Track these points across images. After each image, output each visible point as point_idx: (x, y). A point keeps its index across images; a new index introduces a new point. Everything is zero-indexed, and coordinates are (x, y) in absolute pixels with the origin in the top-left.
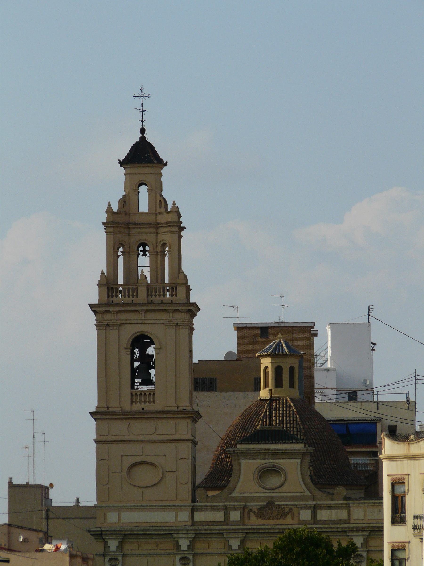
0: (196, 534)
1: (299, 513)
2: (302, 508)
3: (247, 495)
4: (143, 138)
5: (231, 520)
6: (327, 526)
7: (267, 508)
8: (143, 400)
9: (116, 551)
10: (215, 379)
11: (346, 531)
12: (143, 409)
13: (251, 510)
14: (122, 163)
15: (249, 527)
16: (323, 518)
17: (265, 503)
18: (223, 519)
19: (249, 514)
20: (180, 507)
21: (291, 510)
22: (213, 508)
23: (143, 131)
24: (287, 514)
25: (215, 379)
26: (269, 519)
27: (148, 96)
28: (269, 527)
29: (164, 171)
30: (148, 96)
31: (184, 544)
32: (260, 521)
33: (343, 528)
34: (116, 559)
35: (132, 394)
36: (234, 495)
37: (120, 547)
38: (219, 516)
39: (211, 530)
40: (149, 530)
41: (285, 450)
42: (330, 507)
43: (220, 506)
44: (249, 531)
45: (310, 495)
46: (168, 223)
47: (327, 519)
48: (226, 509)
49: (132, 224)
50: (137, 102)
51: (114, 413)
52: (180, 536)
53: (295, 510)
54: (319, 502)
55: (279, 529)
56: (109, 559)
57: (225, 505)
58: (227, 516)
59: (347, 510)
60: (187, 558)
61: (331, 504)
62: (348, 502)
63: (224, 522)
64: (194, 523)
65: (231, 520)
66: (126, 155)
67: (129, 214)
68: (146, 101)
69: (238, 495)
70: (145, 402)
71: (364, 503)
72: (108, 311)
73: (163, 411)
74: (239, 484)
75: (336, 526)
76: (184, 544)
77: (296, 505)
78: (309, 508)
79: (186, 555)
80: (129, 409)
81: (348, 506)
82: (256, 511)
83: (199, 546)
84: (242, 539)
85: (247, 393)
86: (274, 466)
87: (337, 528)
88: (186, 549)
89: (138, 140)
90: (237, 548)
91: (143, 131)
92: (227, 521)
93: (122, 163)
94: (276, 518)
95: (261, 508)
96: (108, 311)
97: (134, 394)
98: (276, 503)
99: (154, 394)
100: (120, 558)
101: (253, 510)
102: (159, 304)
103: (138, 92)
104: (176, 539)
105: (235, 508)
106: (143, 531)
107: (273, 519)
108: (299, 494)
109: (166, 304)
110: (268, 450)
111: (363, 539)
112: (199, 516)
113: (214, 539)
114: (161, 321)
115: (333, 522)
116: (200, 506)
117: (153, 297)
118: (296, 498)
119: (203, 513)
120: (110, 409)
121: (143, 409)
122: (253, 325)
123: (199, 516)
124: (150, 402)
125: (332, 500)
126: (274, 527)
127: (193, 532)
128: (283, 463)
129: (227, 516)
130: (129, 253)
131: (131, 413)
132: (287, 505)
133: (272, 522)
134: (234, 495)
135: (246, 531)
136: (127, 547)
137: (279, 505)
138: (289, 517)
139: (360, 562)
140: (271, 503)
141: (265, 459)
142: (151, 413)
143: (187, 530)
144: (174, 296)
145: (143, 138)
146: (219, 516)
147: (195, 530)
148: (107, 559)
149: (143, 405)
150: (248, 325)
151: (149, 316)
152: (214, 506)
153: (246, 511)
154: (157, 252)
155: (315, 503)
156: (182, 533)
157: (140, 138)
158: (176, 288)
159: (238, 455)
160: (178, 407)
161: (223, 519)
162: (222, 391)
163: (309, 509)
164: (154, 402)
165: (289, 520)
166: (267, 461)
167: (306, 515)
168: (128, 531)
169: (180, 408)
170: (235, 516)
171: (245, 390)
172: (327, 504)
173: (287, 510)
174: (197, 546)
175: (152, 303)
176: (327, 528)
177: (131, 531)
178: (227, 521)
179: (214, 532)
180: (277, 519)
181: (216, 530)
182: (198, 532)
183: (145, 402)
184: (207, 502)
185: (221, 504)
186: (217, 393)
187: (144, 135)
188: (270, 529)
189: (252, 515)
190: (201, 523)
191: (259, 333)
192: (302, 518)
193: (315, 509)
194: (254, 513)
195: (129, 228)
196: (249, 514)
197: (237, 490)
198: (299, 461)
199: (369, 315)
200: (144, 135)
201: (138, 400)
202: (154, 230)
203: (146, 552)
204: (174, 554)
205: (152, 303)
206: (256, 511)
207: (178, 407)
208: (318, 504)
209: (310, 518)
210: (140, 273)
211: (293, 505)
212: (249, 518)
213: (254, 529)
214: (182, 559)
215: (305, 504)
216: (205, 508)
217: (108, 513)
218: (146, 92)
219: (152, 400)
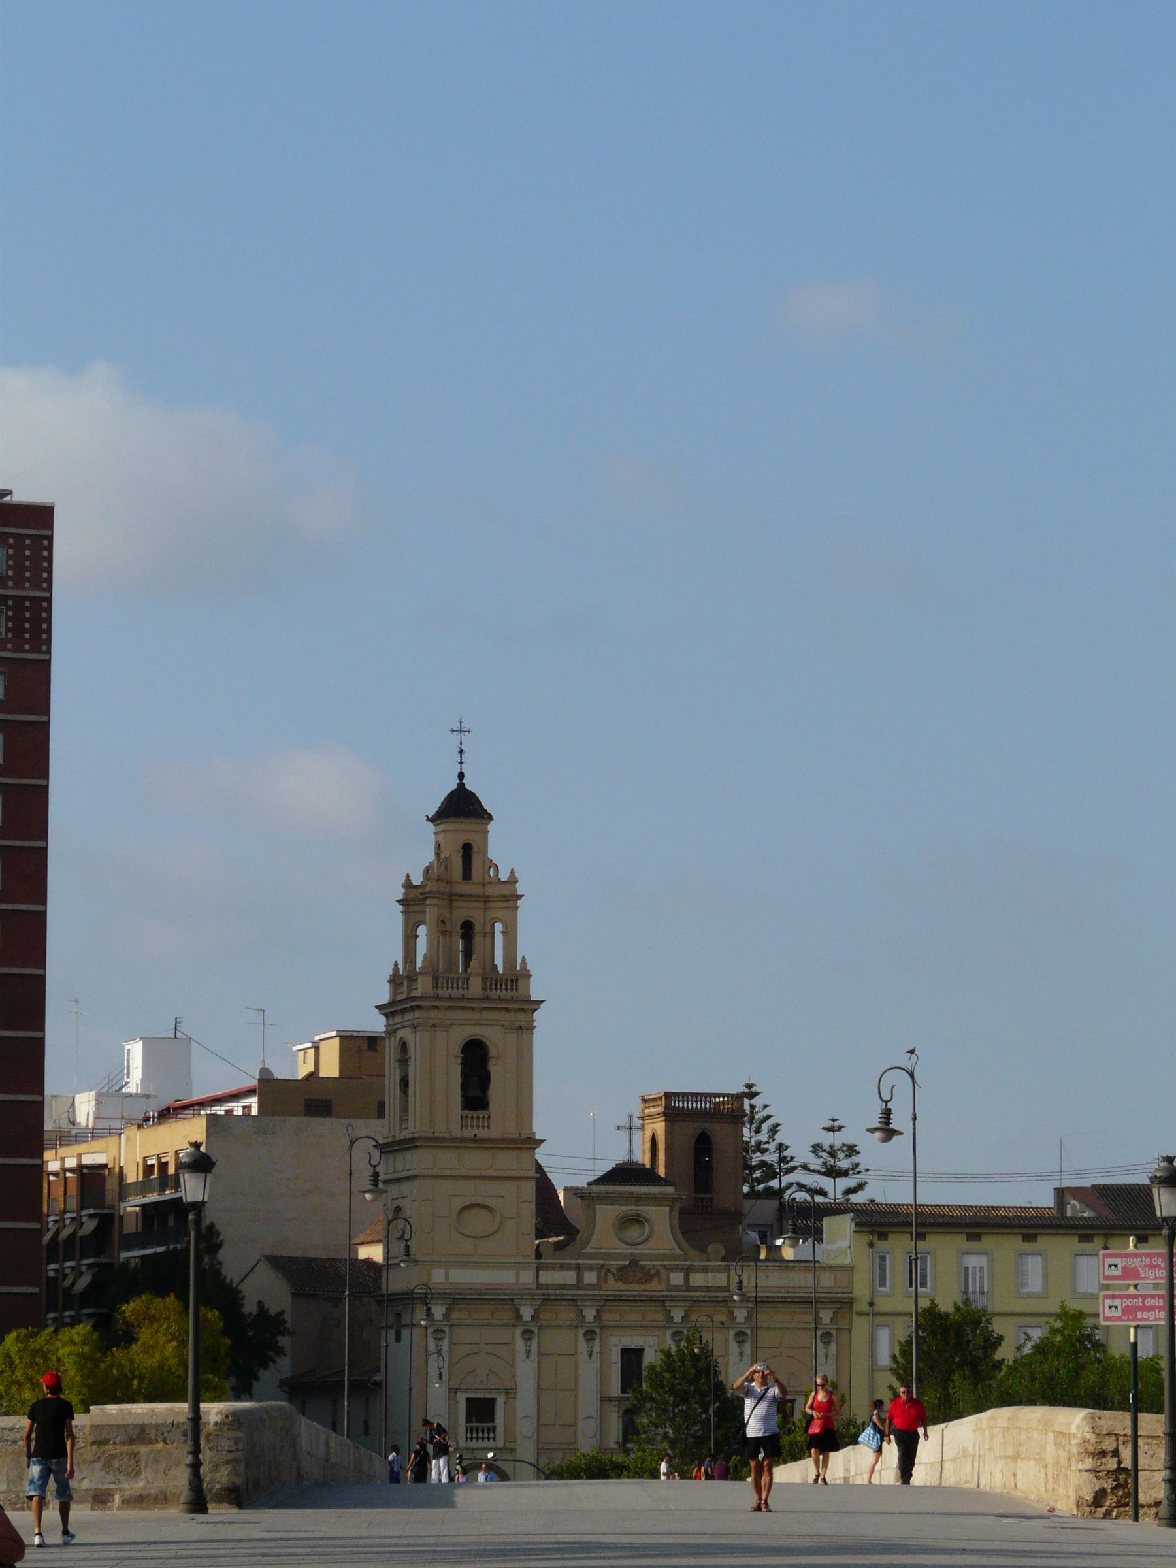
0: (544, 1299)
1: (669, 1277)
2: (672, 1270)
3: (602, 1251)
4: (461, 786)
5: (585, 1283)
6: (703, 1294)
7: (629, 1269)
8: (475, 1124)
9: (681, 1323)
10: (330, 1101)
11: (727, 1301)
12: (475, 1135)
13: (609, 1271)
14: (433, 820)
15: (611, 1293)
16: (698, 1284)
17: (627, 1263)
18: (574, 1282)
19: (606, 1275)
20: (524, 1266)
21: (658, 1273)
22: (562, 1267)
23: (461, 776)
24: (654, 1276)
25: (330, 1101)
26: (631, 1283)
27: (469, 732)
28: (635, 1293)
29: (491, 826)
30: (469, 732)
31: (527, 1312)
32: (621, 1285)
33: (724, 1297)
34: (443, 1331)
35: (461, 1116)
36: (588, 1250)
37: (446, 1316)
38: (570, 1277)
39: (564, 1295)
40: (486, 1294)
41: (654, 1194)
42: (705, 1270)
43: (571, 1264)
44: (609, 1298)
45: (681, 1253)
46: (505, 896)
47: (702, 1285)
48: (578, 1268)
49: (456, 895)
50: (456, 736)
51: (443, 1139)
52: (524, 1302)
53: (663, 1272)
54: (694, 1263)
55: (646, 1296)
56: (435, 1331)
57: (578, 1264)
58: (580, 1277)
59: (726, 1274)
60: (531, 1332)
61: (707, 1266)
62: (729, 1263)
63: (1074, 1290)
64: (539, 1286)
65: (585, 1283)
66: (437, 809)
67: (452, 883)
68: (465, 737)
69: (593, 1251)
70: (478, 1127)
71: (749, 1266)
72: (437, 1007)
73: (502, 1139)
74: (594, 1237)
75: (713, 1294)
76: (527, 1312)
77: (665, 1266)
78: (681, 1270)
79: (680, 1329)
80: (459, 1136)
81: (728, 1269)
82: (615, 1272)
83: (609, 1317)
84: (686, 1308)
85: (368, 1120)
86: (638, 1215)
87: (718, 1297)
88: (530, 1319)
89: (455, 787)
90: (680, 1321)
91: (461, 776)
92: (579, 1285)
93: (433, 820)
94: (640, 1282)
95: (622, 1269)
96: (437, 1007)
97: (464, 1115)
98: (641, 1263)
99: (489, 1116)
100: (447, 1329)
101: (612, 1270)
102: (494, 1000)
103: (456, 726)
104: (518, 1307)
105: (590, 1268)
106: (478, 1294)
107: (637, 1283)
108: (668, 1252)
109: (442, 998)
110: (632, 1193)
111: (683, 1312)
112: (547, 1277)
113: (563, 1307)
114: (500, 1023)
115: (708, 1289)
116: (547, 1263)
117: (489, 991)
118: (664, 1257)
119: (550, 1273)
120: (436, 1135)
121: (475, 1135)
122: (360, 1034)
123: (547, 1277)
124: (483, 1127)
125: (707, 1261)
126: (641, 1293)
127: (540, 1297)
128: (650, 1211)
129: (580, 1277)
130: (451, 932)
131: (462, 1140)
132: (654, 1265)
133: (635, 1286)
134: (588, 1250)
135: (606, 1298)
136: (455, 1315)
137: (644, 1265)
138: (656, 1280)
139: (743, 1341)
140: (634, 1263)
141: (627, 1205)
142: (483, 1140)
143: (533, 1295)
144: (514, 991)
145: (461, 786)
146: (570, 1277)
147: (543, 1295)
148: (819, 1333)
149: (475, 1131)
150: (354, 1034)
151: (487, 1015)
152: (564, 1264)
153: (604, 1271)
154: (485, 934)
155: (688, 1263)
156: (526, 1299)
157: (458, 784)
158: (517, 981)
159: (593, 1199)
160: (520, 1134)
161: (574, 1282)
162: (338, 1116)
163: (681, 1272)
164: (488, 1127)
165: (655, 1285)
166: (629, 1208)
167: (677, 1279)
168: (460, 1294)
169: (523, 1136)
170: (590, 1278)
171: (366, 1116)
172: (702, 1266)
173: (653, 1272)
174: (606, 1316)
175: (437, 997)
176: (704, 1296)
177: (463, 1294)
178: (579, 1285)
179: (565, 1298)
180: (643, 1284)
181: (568, 1295)
182: (546, 1297)
183: (478, 1127)
184: (555, 1259)
185: (573, 1262)
186: (332, 1120)
187: (463, 781)
188: (636, 1296)
189: (610, 1276)
190: (547, 1286)
191: (365, 1045)
192: (672, 1282)
193: (688, 1271)
194: (613, 1274)
195: (451, 901)
196: (606, 1275)
197: (591, 1245)
198: (667, 1209)
199: (176, 1029)
200: (463, 781)
201: (469, 1124)
202: (482, 905)
203: (501, 1323)
204: (577, 1327)
205: (487, 998)
206: (615, 1272)
207: (520, 1134)
208: (692, 1265)
209: (682, 1284)
210: (519, 961)
211: (661, 1266)
212: (606, 1283)
213: (616, 1296)
214: (587, 1333)
215: (677, 1265)
216: (552, 1267)
217: (434, 1271)
218: (466, 726)
219: (486, 1125)
